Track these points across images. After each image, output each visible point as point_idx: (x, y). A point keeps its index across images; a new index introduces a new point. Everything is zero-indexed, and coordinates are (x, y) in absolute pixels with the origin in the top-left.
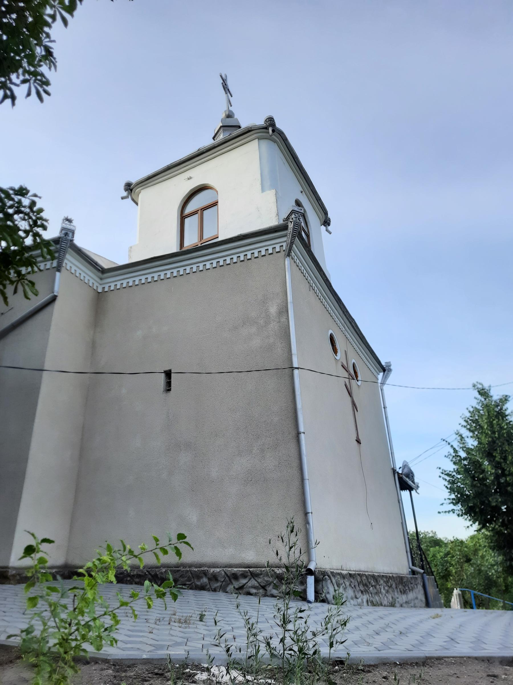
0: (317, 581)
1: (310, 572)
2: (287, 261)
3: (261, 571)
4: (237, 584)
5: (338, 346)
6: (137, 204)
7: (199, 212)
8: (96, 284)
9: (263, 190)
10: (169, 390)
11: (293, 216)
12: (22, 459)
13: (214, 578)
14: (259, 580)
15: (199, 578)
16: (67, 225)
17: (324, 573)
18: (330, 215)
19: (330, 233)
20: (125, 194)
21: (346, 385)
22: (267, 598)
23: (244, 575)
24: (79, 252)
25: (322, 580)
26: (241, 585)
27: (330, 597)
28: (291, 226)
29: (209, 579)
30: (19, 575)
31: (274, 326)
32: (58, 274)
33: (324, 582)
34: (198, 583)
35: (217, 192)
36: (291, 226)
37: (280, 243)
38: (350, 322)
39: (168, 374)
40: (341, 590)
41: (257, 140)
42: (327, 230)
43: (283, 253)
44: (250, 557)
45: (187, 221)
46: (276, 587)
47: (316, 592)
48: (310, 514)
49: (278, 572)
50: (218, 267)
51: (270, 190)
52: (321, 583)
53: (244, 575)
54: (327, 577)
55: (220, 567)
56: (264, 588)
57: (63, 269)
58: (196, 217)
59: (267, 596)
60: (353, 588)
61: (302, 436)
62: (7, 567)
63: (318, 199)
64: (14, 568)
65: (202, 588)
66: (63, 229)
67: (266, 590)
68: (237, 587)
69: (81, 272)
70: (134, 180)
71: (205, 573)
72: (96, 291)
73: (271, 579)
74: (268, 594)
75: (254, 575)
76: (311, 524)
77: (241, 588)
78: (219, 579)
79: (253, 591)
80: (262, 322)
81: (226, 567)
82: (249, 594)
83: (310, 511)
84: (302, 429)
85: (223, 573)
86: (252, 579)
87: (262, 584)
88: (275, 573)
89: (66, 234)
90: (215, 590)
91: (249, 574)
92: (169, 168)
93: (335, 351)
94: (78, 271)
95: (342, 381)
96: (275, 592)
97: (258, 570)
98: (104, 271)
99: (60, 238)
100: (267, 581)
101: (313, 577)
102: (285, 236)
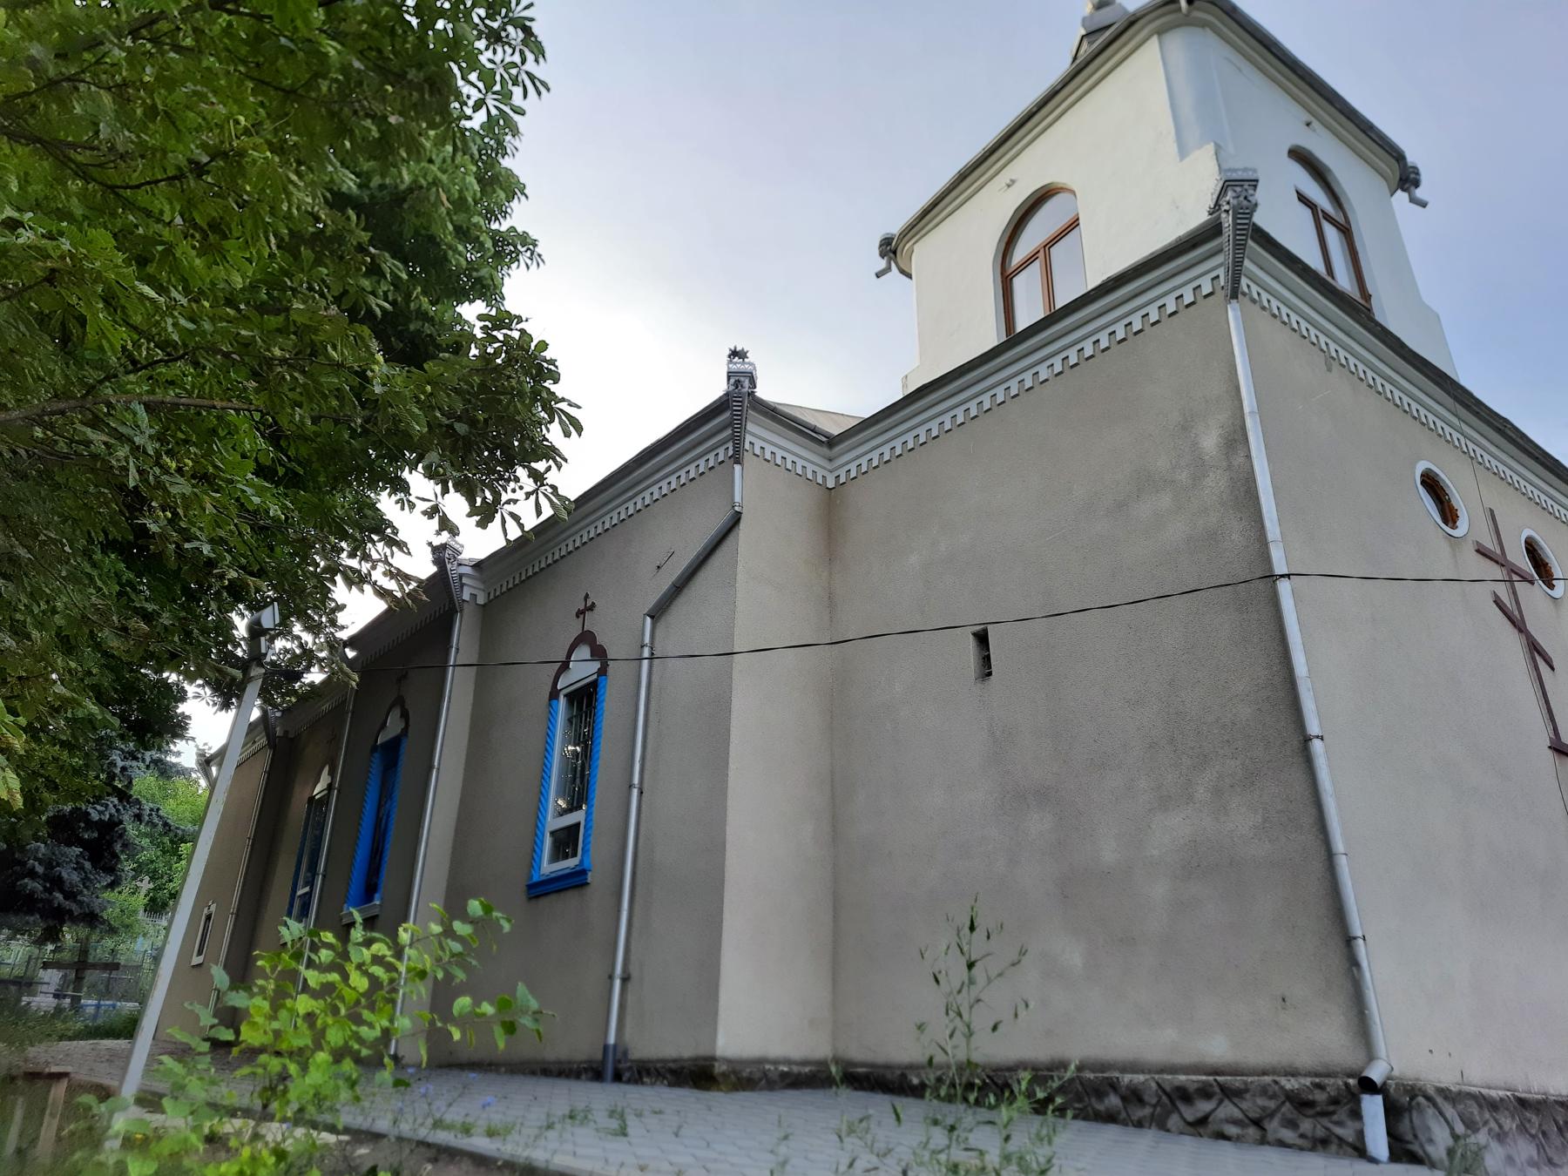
0: (1393, 1112)
1: (1368, 1086)
2: (1233, 313)
3: (1245, 1083)
4: (1190, 1113)
5: (1457, 501)
6: (909, 276)
7: (1041, 254)
8: (820, 473)
9: (1183, 152)
10: (990, 674)
11: (1230, 195)
12: (715, 849)
13: (1134, 1096)
14: (1244, 1105)
15: (1100, 1095)
16: (738, 365)
17: (1413, 1091)
18: (1412, 158)
19: (1424, 205)
20: (883, 264)
21: (1498, 602)
22: (1267, 1147)
23: (1205, 1092)
24: (772, 413)
25: (1409, 1109)
26: (1199, 1115)
27: (1438, 1151)
28: (1227, 221)
29: (1124, 1099)
30: (734, 1072)
31: (1216, 483)
32: (737, 468)
33: (1415, 1114)
34: (1101, 1107)
35: (1073, 193)
36: (1227, 221)
37: (1209, 274)
38: (1499, 431)
39: (982, 638)
40: (1482, 1137)
41: (1155, 39)
42: (1413, 200)
43: (1220, 295)
44: (1217, 1048)
45: (1018, 282)
46: (1292, 1124)
47: (1391, 1133)
48: (1361, 941)
49: (1288, 1087)
50: (1067, 370)
51: (1199, 147)
52: (1406, 1115)
53: (1205, 1092)
54: (1421, 1099)
55: (1150, 1072)
56: (1257, 1123)
57: (747, 457)
58: (1036, 268)
59: (1269, 1143)
60: (1533, 1136)
61: (1317, 745)
62: (713, 1059)
63: (1366, 129)
64: (728, 1061)
65: (1110, 1118)
66: (730, 375)
67: (1264, 1129)
68: (1190, 1118)
69: (785, 454)
70: (895, 229)
71: (1113, 1086)
72: (823, 486)
73: (1272, 1104)
74: (1270, 1137)
75: (1229, 1093)
76: (1364, 964)
77: (1202, 1121)
78: (1146, 1098)
79: (1232, 1130)
80: (1183, 476)
81: (1162, 1071)
82: (1221, 1136)
83: (1360, 934)
84: (1313, 728)
85: (1154, 1085)
86: (1226, 1102)
87: (1251, 1115)
88: (1282, 1088)
89: (737, 384)
90: (1139, 1124)
91: (1217, 1089)
92: (963, 176)
93: (1449, 515)
94: (769, 449)
95: (1483, 594)
96: (1288, 1135)
97: (1236, 1082)
98: (832, 442)
99: (727, 394)
100: (1264, 1109)
101: (1379, 1099)
102: (1221, 251)
